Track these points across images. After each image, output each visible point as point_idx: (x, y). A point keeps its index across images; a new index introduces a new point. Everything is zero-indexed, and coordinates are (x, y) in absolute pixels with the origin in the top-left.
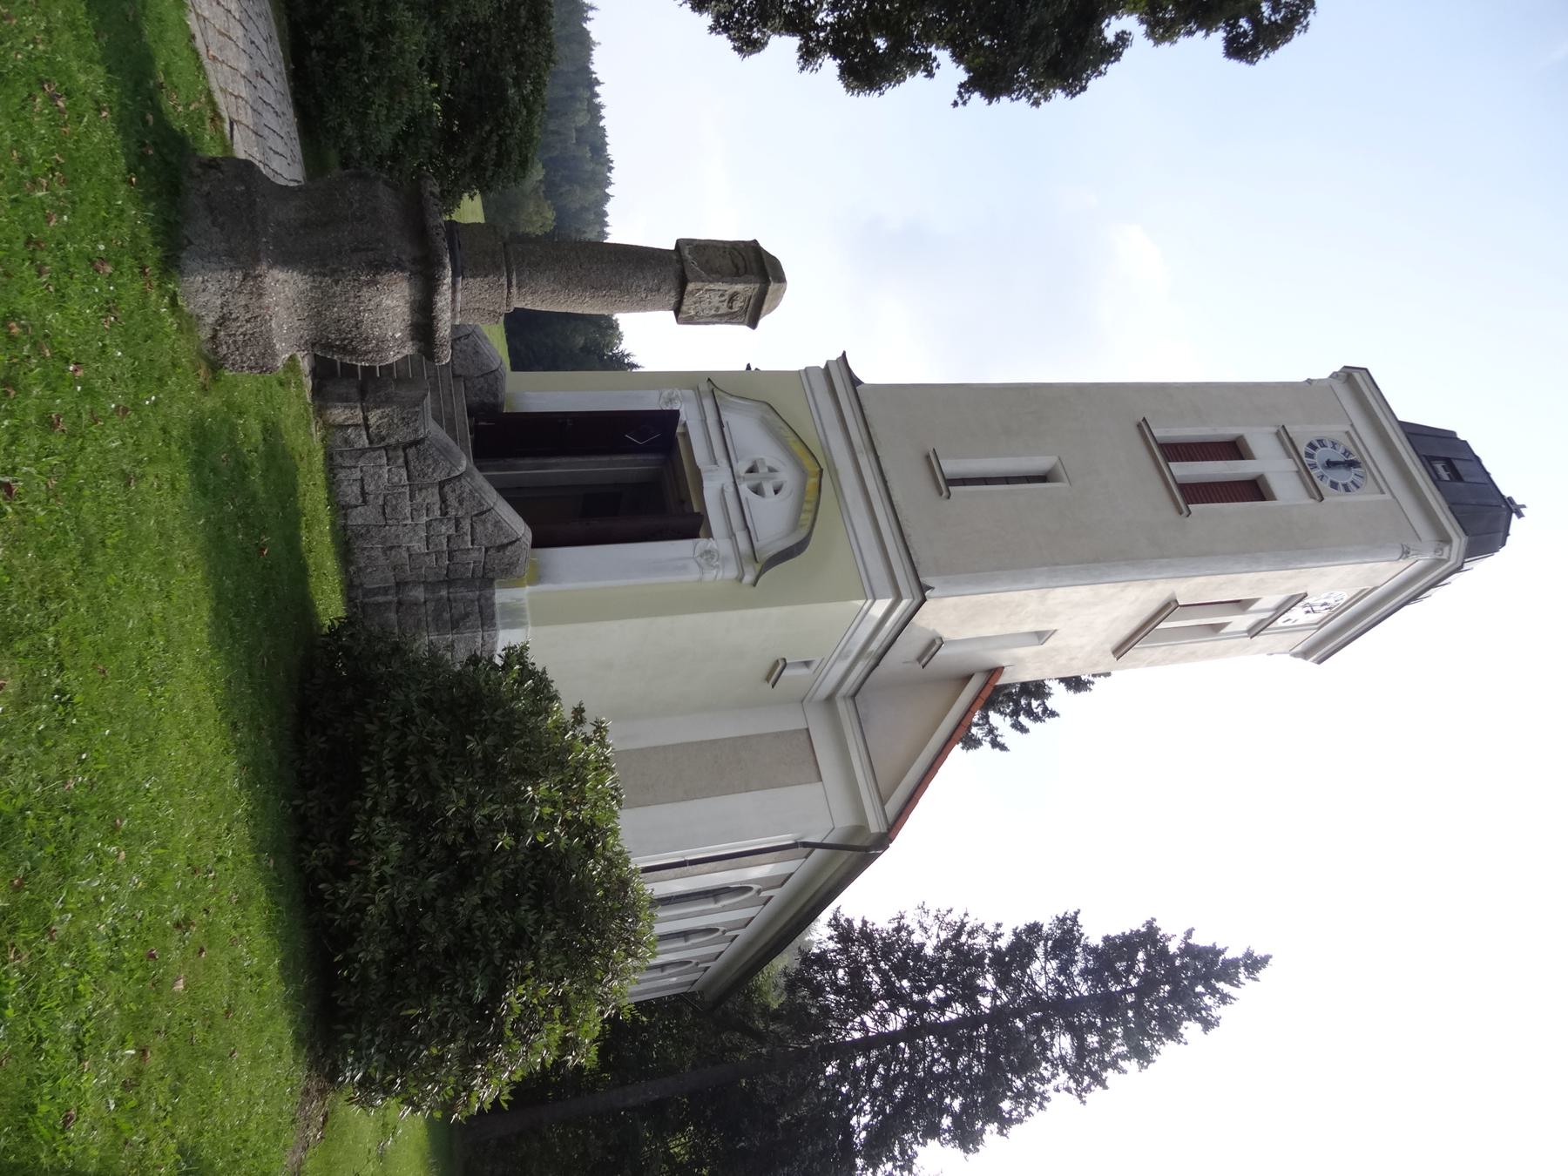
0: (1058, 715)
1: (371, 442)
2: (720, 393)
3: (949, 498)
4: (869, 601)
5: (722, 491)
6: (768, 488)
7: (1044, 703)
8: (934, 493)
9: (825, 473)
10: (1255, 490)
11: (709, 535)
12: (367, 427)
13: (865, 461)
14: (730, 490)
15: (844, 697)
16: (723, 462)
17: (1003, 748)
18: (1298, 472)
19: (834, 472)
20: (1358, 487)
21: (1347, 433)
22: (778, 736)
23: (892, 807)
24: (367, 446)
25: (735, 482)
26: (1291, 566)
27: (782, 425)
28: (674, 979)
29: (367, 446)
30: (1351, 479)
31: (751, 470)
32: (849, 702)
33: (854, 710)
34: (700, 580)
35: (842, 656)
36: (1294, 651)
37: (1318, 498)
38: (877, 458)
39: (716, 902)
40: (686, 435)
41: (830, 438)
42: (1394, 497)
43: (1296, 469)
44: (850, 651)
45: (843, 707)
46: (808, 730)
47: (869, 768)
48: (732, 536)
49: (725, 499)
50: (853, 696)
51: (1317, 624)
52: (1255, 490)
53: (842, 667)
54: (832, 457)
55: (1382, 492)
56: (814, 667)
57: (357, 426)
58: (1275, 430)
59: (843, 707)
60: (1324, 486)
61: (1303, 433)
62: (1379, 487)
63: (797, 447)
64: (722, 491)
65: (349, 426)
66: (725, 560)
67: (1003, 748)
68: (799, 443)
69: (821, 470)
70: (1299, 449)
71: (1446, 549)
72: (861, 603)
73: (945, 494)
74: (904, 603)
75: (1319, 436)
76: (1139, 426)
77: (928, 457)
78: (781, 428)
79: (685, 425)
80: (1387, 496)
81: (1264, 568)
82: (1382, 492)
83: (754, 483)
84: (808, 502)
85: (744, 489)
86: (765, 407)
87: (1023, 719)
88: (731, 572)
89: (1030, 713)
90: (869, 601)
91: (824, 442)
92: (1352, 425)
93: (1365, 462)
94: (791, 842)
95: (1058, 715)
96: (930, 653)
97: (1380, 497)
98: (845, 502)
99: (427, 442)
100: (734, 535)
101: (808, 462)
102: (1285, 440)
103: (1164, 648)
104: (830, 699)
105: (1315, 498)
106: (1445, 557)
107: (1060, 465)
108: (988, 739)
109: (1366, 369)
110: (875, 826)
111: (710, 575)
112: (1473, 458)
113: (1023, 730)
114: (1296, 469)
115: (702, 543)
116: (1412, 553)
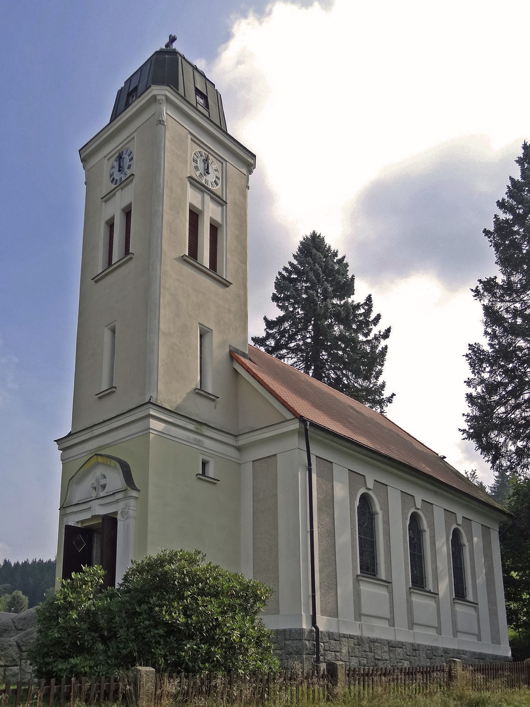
0: (370, 296)
1: (16, 665)
2: (64, 505)
3: (116, 387)
4: (151, 431)
5: (101, 505)
6: (103, 482)
7: (362, 305)
8: (113, 396)
9: (96, 453)
10: (128, 213)
11: (116, 513)
12: (6, 666)
13: (97, 431)
14: (100, 501)
15: (237, 441)
16: (90, 503)
17: (388, 331)
18: (122, 189)
19: (101, 448)
20: (131, 152)
21: (108, 160)
22: (254, 478)
23: (289, 416)
24: (19, 667)
25: (98, 499)
26: (161, 192)
27: (78, 474)
28: (475, 539)
29: (19, 667)
30: (127, 157)
31: (95, 488)
32: (239, 438)
33: (243, 436)
34: (135, 518)
35: (199, 443)
36: (246, 173)
37: (132, 177)
38: (95, 425)
39: (377, 514)
40: (82, 522)
41: (88, 450)
42: (136, 131)
43: (120, 190)
44: (195, 440)
45: (242, 441)
46: (253, 461)
47: (270, 428)
48: (117, 501)
49: (104, 504)
50: (236, 436)
51: (222, 163)
52: (128, 213)
53: (207, 442)
54: (95, 449)
55: (134, 138)
56: (207, 458)
57: (5, 670)
58: (104, 203)
59: (242, 441)
60: (129, 173)
61: (107, 186)
62: (131, 140)
63: (87, 467)
64: (101, 505)
65: (5, 674)
66: (127, 505)
67: (388, 331)
68: (85, 466)
69: (96, 454)
70: (115, 187)
71: (158, 97)
72: (152, 436)
73: (114, 390)
74: (152, 412)
75: (108, 176)
76: (96, 282)
77: (100, 398)
78: (79, 474)
79: (78, 522)
80: (135, 135)
81: (161, 208)
82: (134, 138)
83: (100, 488)
84: (107, 462)
85: (102, 494)
86: (71, 481)
87: (373, 316)
88: (132, 502)
89: (369, 311)
90: (151, 431)
91: (89, 452)
92: (105, 157)
93: (119, 150)
94: (307, 472)
95: (370, 296)
96: (206, 395)
97: (135, 138)
98: (112, 442)
99: (19, 641)
100: (117, 500)
101: (93, 461)
102: (108, 197)
103: (228, 256)
104: (239, 449)
105: (133, 179)
106: (163, 98)
107: (109, 326)
108: (382, 340)
109: (79, 151)
110: (296, 425)
111: (132, 513)
112: (130, 80)
113: (378, 317)
114: (120, 190)
115: (119, 517)
116: (161, 119)
